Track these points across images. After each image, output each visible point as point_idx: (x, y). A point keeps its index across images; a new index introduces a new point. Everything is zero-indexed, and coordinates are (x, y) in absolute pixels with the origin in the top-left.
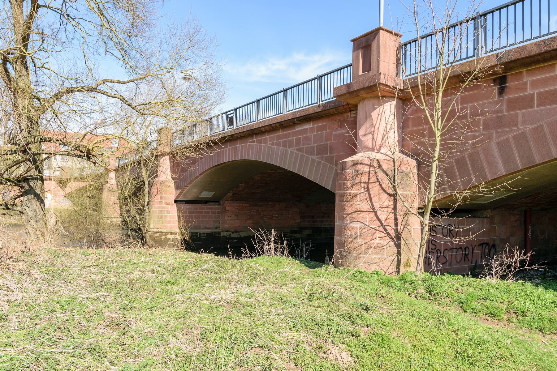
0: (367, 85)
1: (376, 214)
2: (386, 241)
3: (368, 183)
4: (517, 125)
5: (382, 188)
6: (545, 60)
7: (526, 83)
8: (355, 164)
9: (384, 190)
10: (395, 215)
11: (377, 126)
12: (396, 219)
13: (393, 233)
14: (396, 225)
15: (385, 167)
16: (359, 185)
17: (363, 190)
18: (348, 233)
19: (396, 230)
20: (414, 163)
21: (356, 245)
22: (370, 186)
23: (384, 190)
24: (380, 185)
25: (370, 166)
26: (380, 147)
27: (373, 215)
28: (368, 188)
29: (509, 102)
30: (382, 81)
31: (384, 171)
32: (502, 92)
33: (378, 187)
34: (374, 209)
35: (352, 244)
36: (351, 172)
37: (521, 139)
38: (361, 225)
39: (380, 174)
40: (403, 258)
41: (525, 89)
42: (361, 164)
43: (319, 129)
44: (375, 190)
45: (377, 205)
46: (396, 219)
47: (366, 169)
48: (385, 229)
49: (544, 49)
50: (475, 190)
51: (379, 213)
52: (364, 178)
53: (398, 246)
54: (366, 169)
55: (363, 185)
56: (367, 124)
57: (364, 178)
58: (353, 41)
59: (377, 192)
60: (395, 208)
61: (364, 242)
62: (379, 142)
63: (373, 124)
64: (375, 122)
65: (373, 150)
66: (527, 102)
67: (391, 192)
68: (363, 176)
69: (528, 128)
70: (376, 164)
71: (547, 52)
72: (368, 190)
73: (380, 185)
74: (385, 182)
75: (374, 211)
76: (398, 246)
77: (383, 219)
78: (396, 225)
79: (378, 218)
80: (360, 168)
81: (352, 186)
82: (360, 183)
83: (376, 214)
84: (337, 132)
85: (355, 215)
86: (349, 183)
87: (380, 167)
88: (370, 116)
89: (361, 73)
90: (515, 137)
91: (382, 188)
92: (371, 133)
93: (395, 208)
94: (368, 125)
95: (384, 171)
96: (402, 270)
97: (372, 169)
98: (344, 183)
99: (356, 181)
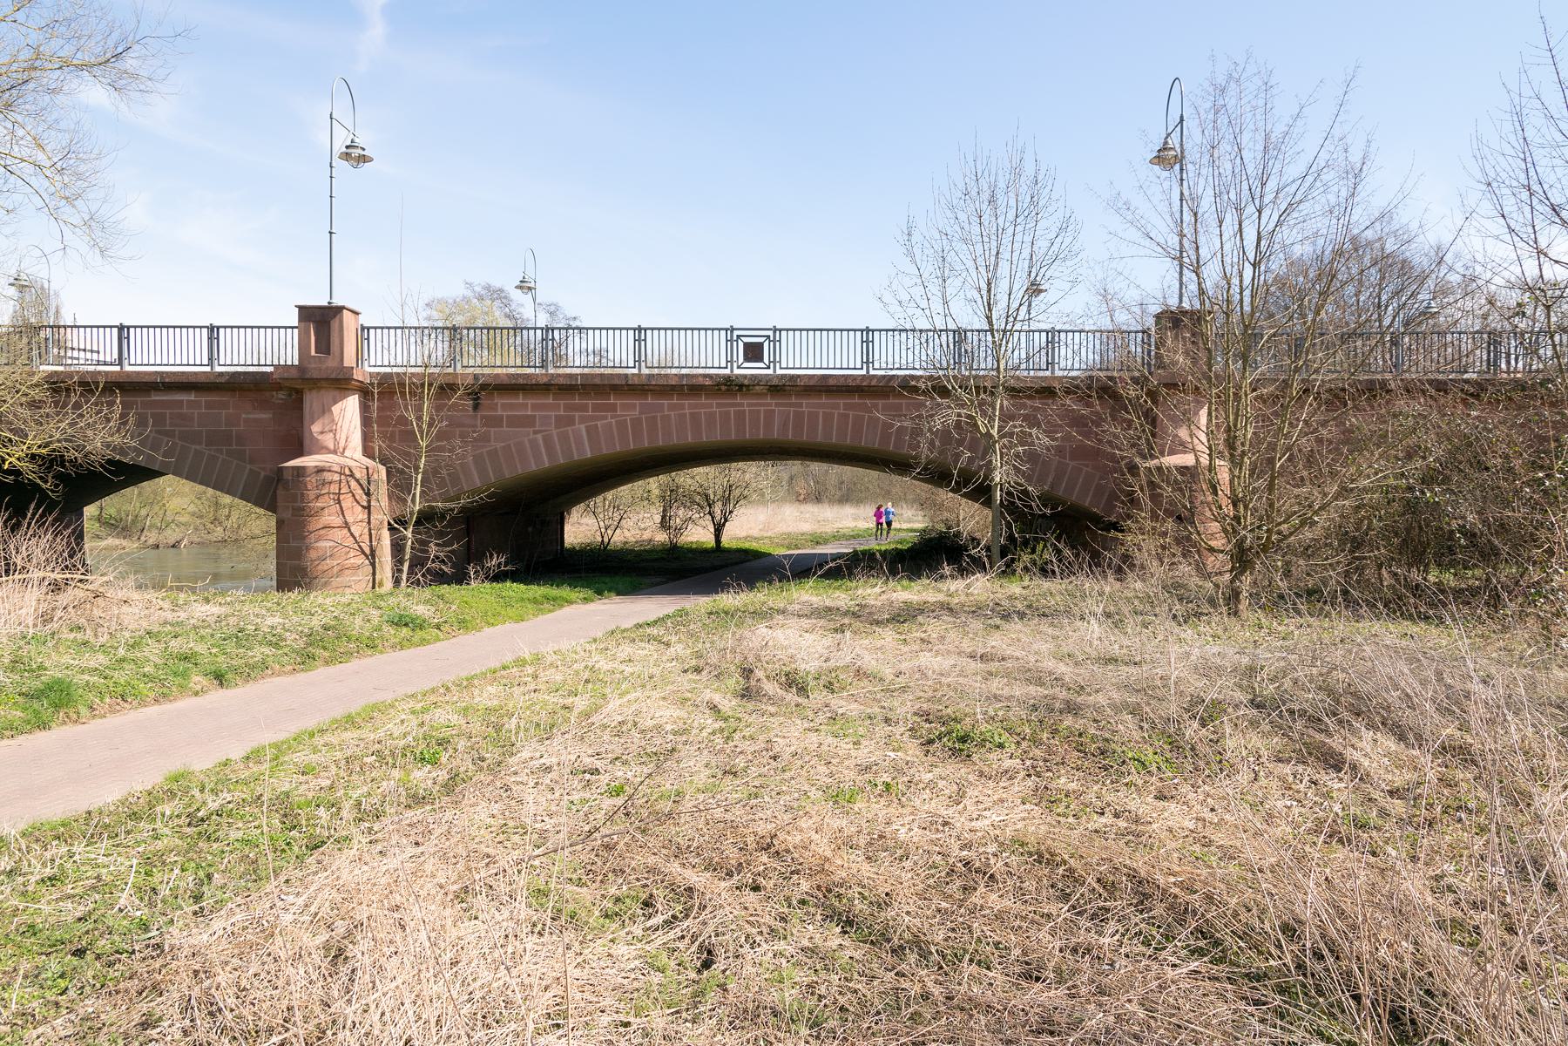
0: (333, 376)
1: (349, 530)
2: (361, 560)
3: (339, 494)
4: (489, 441)
5: (356, 500)
6: (508, 390)
7: (497, 404)
8: (320, 470)
9: (358, 502)
10: (370, 529)
11: (339, 425)
12: (370, 535)
13: (367, 551)
14: (371, 541)
15: (358, 475)
16: (326, 497)
17: (332, 502)
18: (313, 555)
19: (371, 546)
20: (383, 470)
21: (326, 568)
22: (342, 497)
23: (358, 502)
24: (353, 495)
25: (341, 474)
26: (344, 449)
27: (346, 531)
28: (339, 498)
29: (483, 417)
30: (355, 377)
31: (357, 481)
32: (476, 407)
33: (351, 499)
34: (346, 523)
35: (320, 567)
36: (314, 480)
37: (493, 454)
38: (332, 544)
39: (353, 483)
40: (378, 577)
41: (496, 410)
42: (330, 471)
43: (209, 406)
44: (347, 502)
45: (350, 519)
46: (370, 535)
47: (336, 477)
48: (360, 547)
49: (513, 382)
50: (1459, 538)
51: (352, 529)
52: (334, 488)
53: (373, 565)
54: (336, 477)
55: (332, 496)
56: (326, 419)
57: (334, 488)
58: (301, 308)
59: (350, 505)
60: (369, 523)
61: (335, 563)
62: (342, 444)
63: (333, 420)
64: (336, 419)
65: (335, 452)
66: (496, 422)
67: (365, 504)
68: (332, 486)
69: (500, 445)
70: (347, 472)
71: (515, 385)
72: (339, 502)
73: (353, 495)
74: (359, 492)
75: (347, 525)
76: (373, 565)
77: (357, 535)
78: (371, 541)
79: (352, 534)
80: (328, 476)
81: (317, 498)
82: (329, 493)
83: (349, 530)
84: (251, 416)
85: (322, 532)
86: (312, 494)
87: (352, 475)
88: (330, 411)
89: (313, 353)
90: (487, 452)
91: (356, 500)
92: (331, 431)
93: (369, 523)
94: (326, 421)
95: (357, 481)
96: (377, 588)
97: (343, 477)
98: (302, 494)
99: (323, 492)
